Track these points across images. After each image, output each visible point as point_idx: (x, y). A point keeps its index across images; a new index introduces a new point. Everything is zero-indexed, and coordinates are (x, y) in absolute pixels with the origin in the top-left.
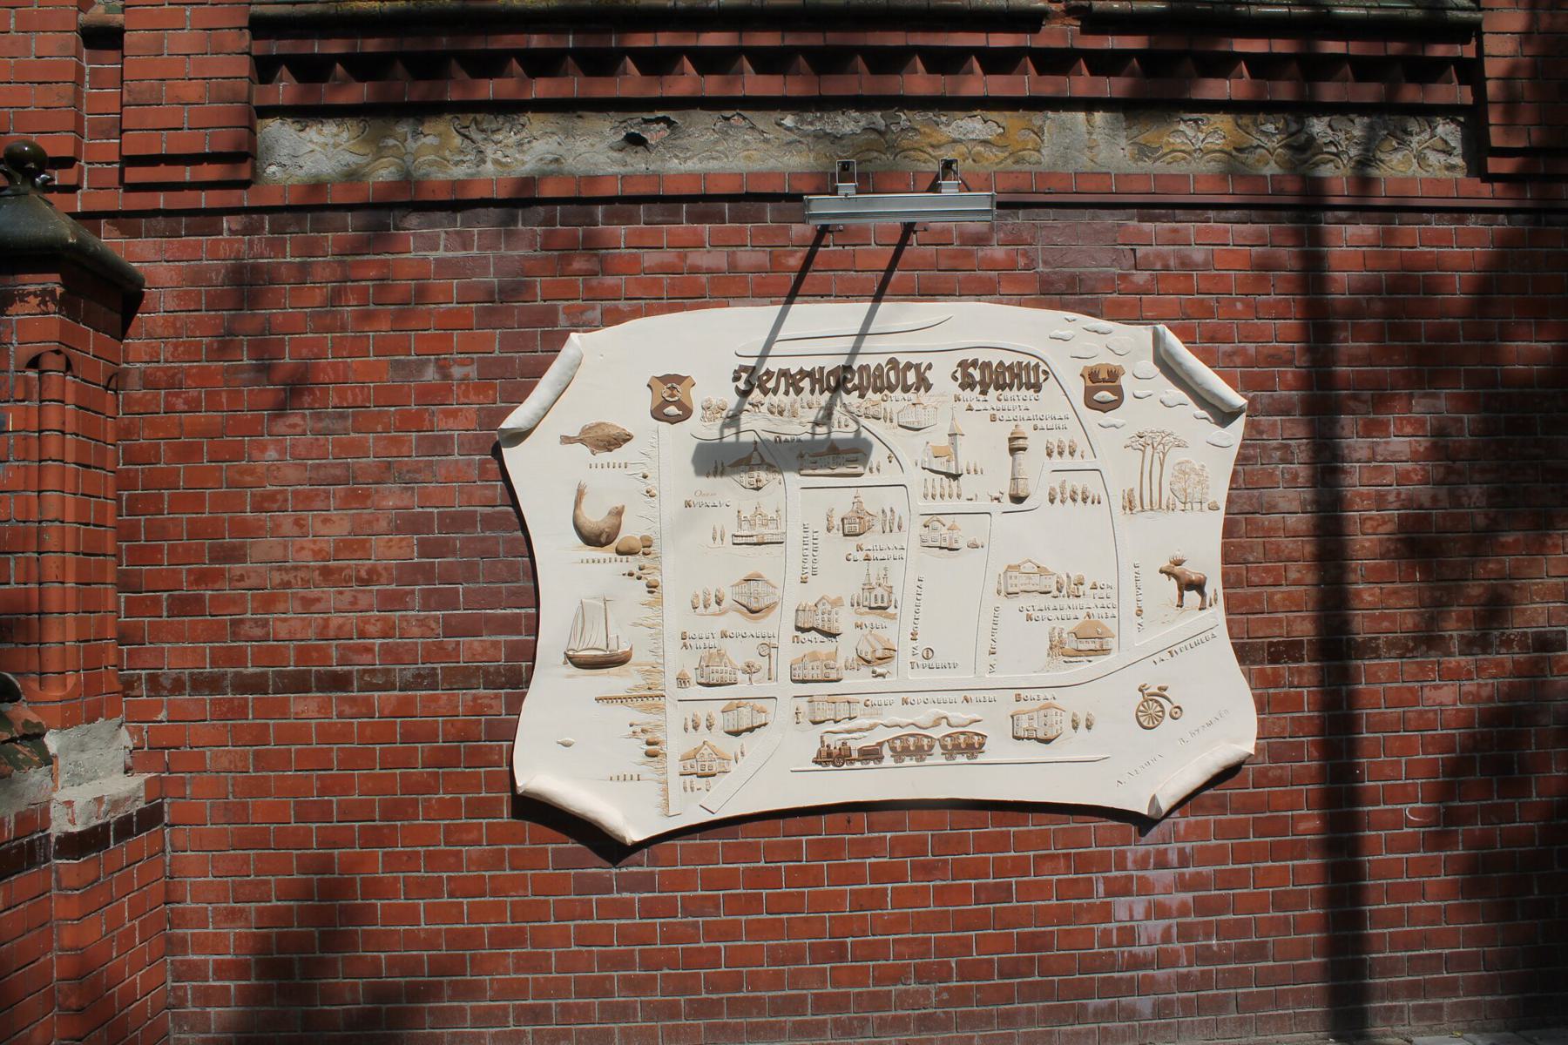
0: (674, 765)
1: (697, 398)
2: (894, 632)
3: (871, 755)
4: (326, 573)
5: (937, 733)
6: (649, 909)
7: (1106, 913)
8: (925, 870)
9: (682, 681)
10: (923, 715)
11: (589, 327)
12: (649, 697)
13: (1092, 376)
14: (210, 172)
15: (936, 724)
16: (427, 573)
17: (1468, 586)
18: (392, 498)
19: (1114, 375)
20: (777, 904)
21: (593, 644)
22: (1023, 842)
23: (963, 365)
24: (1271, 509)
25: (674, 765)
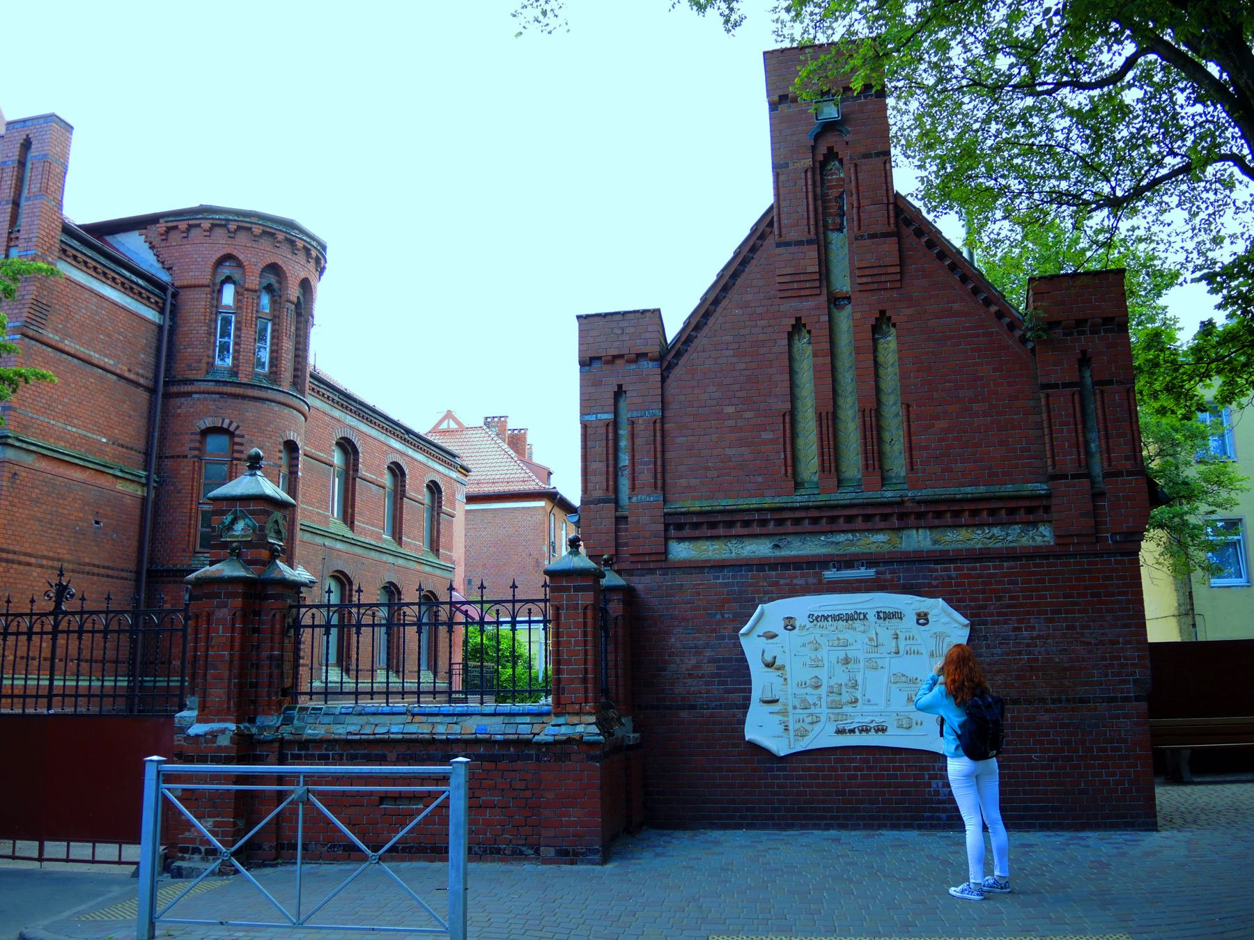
0: (792, 733)
1: (797, 624)
2: (859, 695)
3: (852, 731)
4: (689, 675)
5: (872, 725)
6: (786, 777)
7: (929, 785)
8: (870, 769)
9: (795, 708)
10: (868, 719)
11: (765, 602)
12: (784, 713)
13: (919, 615)
14: (653, 558)
15: (872, 722)
16: (719, 675)
17: (158, 582)
18: (708, 653)
19: (926, 614)
20: (824, 777)
21: (768, 697)
22: (901, 761)
23: (878, 612)
24: (981, 655)
25: (792, 733)
